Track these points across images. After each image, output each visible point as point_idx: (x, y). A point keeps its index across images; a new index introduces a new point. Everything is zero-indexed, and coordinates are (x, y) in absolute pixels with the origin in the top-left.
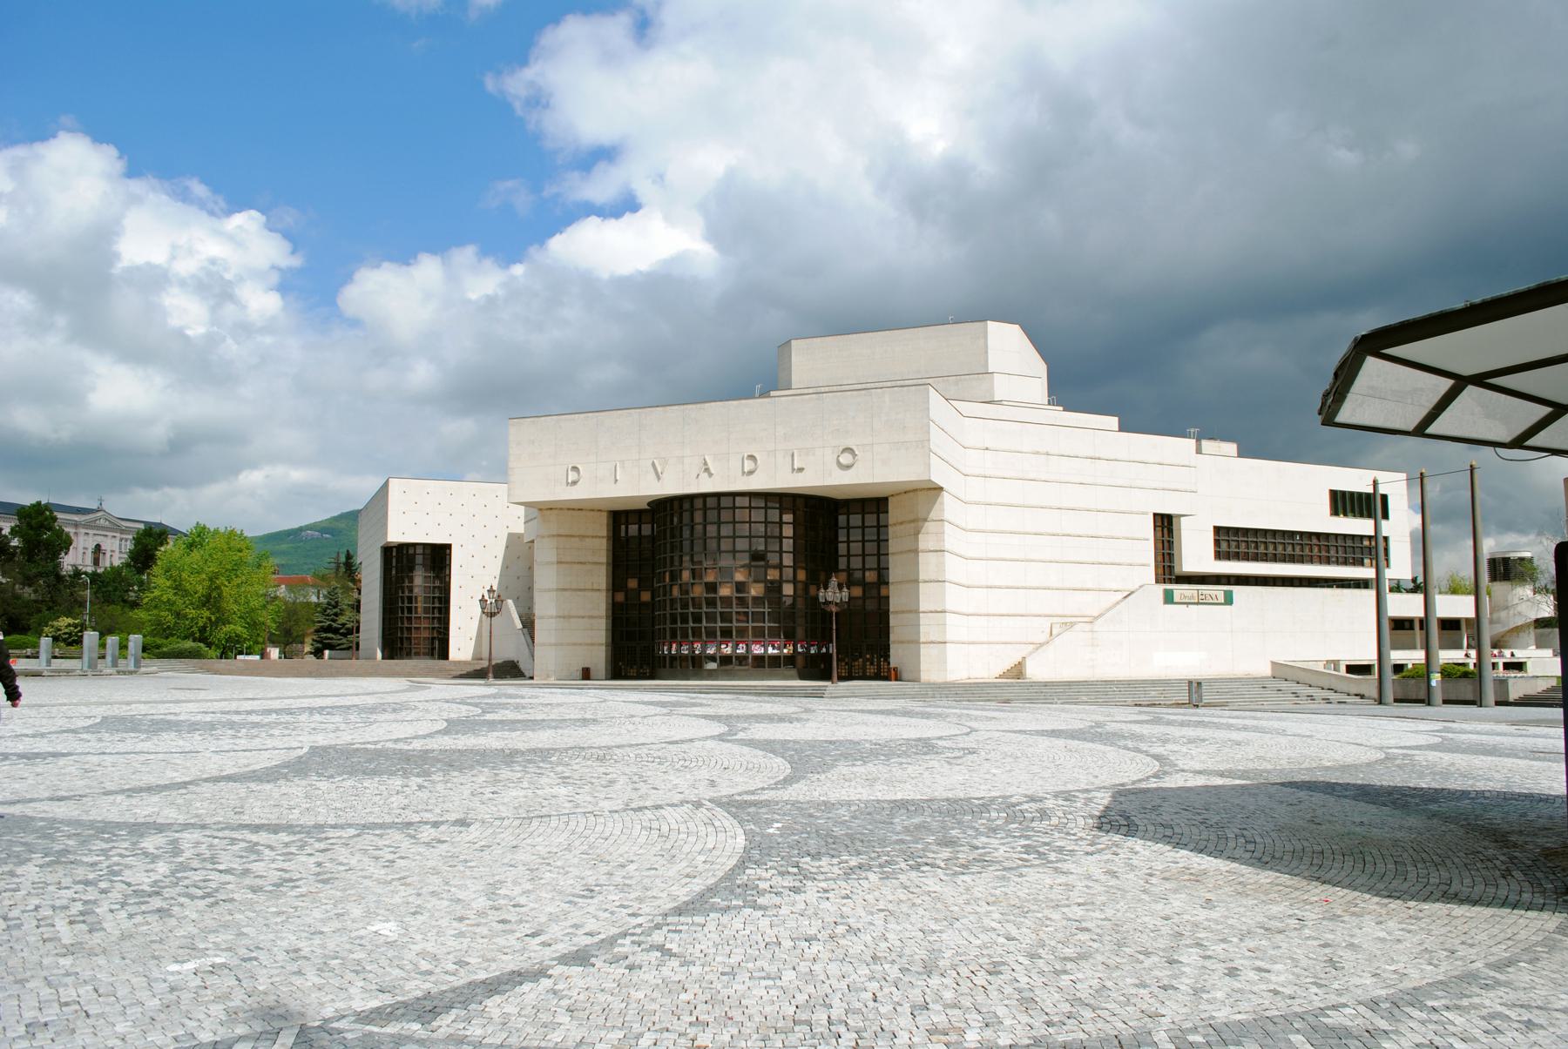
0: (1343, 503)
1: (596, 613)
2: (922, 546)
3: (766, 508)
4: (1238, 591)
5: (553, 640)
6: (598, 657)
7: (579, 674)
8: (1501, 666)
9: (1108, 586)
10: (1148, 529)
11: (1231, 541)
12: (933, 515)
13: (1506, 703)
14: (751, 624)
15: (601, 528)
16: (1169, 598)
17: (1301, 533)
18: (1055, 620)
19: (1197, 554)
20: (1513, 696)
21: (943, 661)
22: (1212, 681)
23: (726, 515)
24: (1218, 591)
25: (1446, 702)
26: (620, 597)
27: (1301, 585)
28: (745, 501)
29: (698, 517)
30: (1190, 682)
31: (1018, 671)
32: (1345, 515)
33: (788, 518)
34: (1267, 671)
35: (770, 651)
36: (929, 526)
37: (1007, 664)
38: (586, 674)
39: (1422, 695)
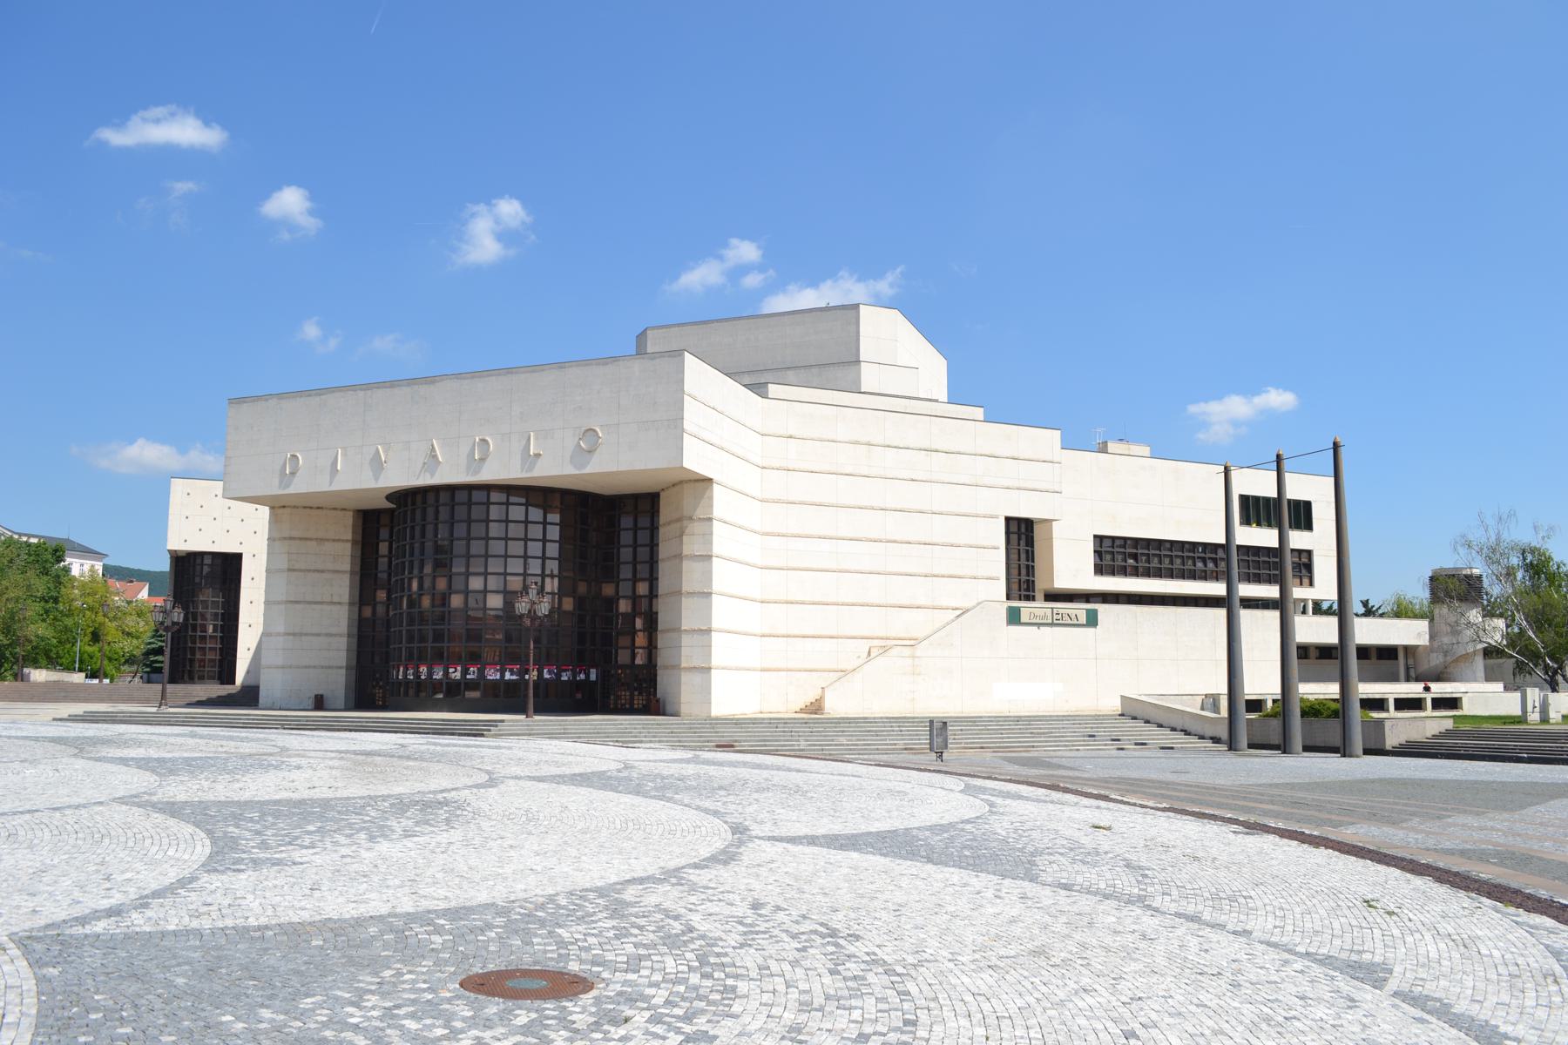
0: (1256, 510)
1: (334, 630)
2: (686, 550)
3: (508, 504)
4: (1104, 610)
5: (280, 662)
6: (337, 682)
7: (311, 703)
8: (1429, 704)
9: (945, 604)
10: (997, 534)
11: (1116, 553)
12: (699, 513)
13: (1381, 752)
14: (430, 645)
15: (345, 529)
16: (1014, 617)
17: (1205, 545)
18: (876, 643)
19: (1071, 564)
20: (1391, 741)
21: (706, 690)
22: (959, 720)
23: (477, 512)
24: (1079, 610)
25: (1307, 749)
26: (368, 612)
27: (1117, 602)
28: (501, 497)
29: (444, 513)
30: (931, 722)
31: (816, 707)
32: (1259, 524)
33: (554, 517)
34: (1114, 705)
35: (508, 676)
36: (695, 527)
37: (810, 697)
38: (319, 703)
39: (1337, 742)
